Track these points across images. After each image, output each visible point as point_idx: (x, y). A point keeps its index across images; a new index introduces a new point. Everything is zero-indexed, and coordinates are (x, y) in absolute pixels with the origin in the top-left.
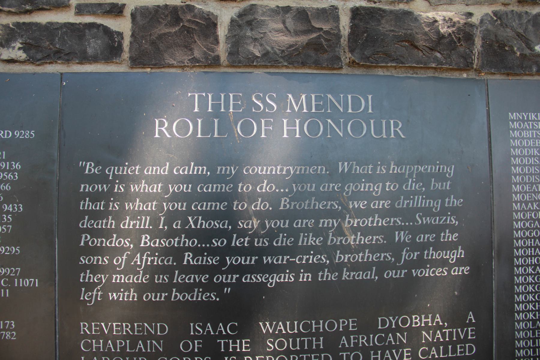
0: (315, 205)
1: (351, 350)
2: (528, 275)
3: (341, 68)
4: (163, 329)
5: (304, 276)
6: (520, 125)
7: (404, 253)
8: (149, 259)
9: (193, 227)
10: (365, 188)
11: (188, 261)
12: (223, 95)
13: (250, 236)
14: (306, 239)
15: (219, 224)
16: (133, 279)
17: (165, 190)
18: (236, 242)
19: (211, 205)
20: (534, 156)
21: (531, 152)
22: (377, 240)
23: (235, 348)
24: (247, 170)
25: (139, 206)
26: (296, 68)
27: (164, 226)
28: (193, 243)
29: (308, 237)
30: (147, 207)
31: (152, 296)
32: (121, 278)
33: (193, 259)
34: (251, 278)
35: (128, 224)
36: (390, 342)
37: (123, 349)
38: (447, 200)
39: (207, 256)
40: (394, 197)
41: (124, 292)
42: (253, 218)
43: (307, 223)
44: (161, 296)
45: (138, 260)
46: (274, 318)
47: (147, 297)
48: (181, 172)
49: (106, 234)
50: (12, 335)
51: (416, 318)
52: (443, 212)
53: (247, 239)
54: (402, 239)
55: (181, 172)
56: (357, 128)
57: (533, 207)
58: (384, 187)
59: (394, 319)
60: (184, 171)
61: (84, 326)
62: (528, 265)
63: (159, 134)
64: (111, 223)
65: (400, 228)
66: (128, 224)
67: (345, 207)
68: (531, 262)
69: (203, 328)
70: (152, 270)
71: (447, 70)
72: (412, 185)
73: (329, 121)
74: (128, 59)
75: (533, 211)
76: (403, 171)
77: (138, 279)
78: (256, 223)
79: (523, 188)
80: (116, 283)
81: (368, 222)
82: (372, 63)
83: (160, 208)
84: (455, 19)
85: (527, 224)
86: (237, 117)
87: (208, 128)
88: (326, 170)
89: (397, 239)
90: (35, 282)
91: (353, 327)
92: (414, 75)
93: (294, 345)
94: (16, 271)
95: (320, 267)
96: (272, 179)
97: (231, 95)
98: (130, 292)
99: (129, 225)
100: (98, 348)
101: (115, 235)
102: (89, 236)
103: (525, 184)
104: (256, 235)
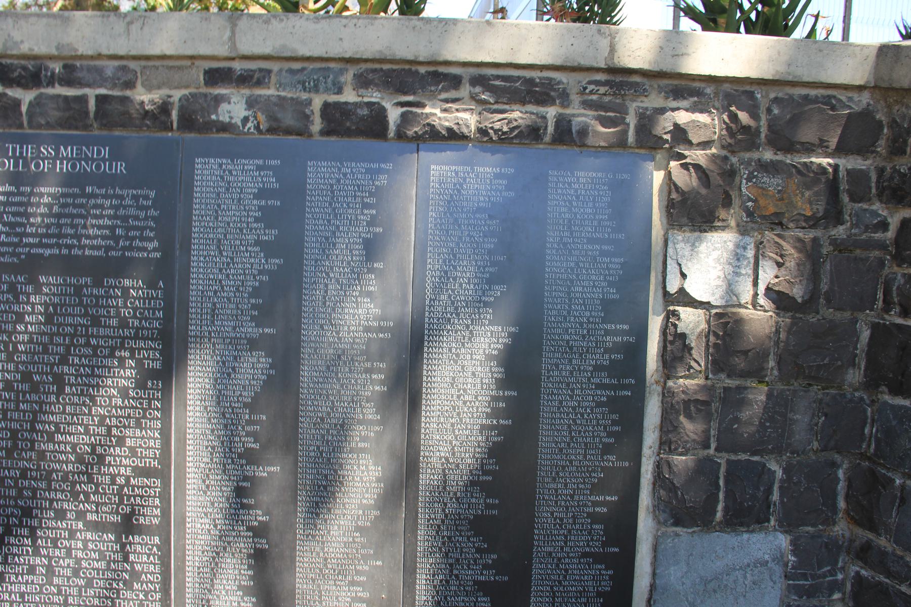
18: (29, 230)
40: (116, 208)
46: (47, 274)
52: (146, 218)
56: (98, 167)
67: (89, 213)
69: (10, 277)
72: (128, 202)
78: (39, 219)
84: (156, 100)
85: (202, 230)
86: (32, 159)
87: (16, 165)
93: (58, 290)
95: (73, 246)
96: (49, 195)
104: (39, 226)
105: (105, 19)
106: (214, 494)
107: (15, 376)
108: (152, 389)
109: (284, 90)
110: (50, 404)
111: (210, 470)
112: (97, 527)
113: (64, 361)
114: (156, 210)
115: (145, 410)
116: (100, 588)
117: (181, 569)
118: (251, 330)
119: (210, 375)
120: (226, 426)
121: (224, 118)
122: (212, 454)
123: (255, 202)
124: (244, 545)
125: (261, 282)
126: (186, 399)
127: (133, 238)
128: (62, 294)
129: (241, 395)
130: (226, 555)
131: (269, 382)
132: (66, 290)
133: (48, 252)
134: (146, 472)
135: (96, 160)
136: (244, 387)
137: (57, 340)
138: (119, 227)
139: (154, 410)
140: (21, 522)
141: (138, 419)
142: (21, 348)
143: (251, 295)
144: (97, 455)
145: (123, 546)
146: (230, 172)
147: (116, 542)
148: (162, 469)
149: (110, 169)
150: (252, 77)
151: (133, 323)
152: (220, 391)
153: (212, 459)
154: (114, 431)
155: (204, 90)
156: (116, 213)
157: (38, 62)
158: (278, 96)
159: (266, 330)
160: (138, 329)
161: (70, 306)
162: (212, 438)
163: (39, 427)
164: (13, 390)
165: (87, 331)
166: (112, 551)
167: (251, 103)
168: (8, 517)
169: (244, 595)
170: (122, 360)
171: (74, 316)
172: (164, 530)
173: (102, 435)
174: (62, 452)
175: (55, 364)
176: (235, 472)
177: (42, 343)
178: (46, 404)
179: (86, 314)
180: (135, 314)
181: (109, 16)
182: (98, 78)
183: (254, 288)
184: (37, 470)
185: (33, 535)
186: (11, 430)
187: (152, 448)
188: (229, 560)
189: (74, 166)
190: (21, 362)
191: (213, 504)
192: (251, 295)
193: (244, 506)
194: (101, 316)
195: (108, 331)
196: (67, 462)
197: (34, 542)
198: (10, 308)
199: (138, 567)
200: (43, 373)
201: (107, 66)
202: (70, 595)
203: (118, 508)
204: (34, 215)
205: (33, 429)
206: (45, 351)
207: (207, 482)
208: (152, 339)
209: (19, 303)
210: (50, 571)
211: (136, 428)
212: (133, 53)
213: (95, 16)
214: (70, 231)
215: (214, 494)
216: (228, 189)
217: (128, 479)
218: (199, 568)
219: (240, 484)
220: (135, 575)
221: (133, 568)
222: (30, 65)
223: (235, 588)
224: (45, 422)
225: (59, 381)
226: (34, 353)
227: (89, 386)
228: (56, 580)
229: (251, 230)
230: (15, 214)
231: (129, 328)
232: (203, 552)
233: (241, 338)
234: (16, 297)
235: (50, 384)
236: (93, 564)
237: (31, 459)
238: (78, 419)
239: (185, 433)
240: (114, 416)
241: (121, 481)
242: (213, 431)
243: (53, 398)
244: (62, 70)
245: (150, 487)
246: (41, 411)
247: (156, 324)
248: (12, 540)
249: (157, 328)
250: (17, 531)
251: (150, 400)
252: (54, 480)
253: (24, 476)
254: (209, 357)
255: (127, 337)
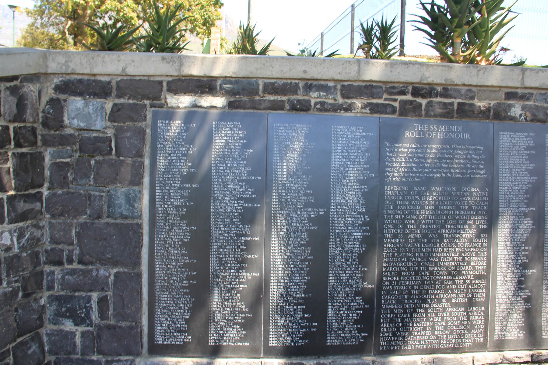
18: (426, 165)
40: (466, 155)
46: (435, 186)
52: (480, 160)
56: (457, 136)
67: (454, 157)
96: (435, 149)
105: (468, 68)
106: (508, 284)
107: (420, 236)
108: (483, 238)
109: (537, 102)
110: (436, 248)
111: (507, 273)
112: (456, 305)
113: (443, 227)
114: (484, 156)
115: (480, 248)
116: (456, 334)
117: (493, 321)
118: (525, 209)
119: (508, 230)
120: (514, 253)
121: (513, 114)
122: (508, 266)
123: (525, 152)
124: (521, 306)
125: (529, 187)
126: (497, 242)
127: (474, 169)
128: (442, 196)
129: (521, 238)
130: (513, 312)
131: (532, 232)
132: (444, 193)
133: (436, 176)
134: (479, 277)
135: (456, 132)
136: (522, 235)
137: (440, 217)
138: (468, 163)
139: (483, 247)
140: (421, 306)
141: (476, 252)
142: (423, 222)
143: (525, 193)
144: (458, 271)
145: (468, 313)
146: (514, 138)
147: (464, 311)
148: (487, 275)
149: (463, 136)
150: (525, 96)
151: (475, 208)
152: (512, 237)
153: (508, 268)
154: (466, 259)
155: (503, 101)
156: (466, 157)
157: (431, 86)
158: (535, 105)
159: (531, 209)
160: (477, 210)
161: (446, 201)
162: (509, 258)
163: (431, 259)
164: (419, 243)
165: (454, 212)
166: (463, 316)
167: (523, 108)
168: (414, 304)
169: (520, 330)
170: (470, 225)
171: (448, 206)
172: (486, 304)
173: (460, 261)
174: (442, 271)
175: (439, 229)
176: (518, 273)
177: (433, 219)
178: (435, 248)
179: (453, 205)
180: (476, 203)
181: (470, 67)
182: (458, 94)
183: (526, 190)
184: (429, 280)
185: (426, 312)
186: (417, 262)
187: (483, 265)
188: (514, 315)
189: (446, 135)
190: (423, 229)
191: (508, 289)
192: (525, 193)
193: (521, 289)
194: (460, 205)
195: (463, 212)
196: (443, 275)
197: (426, 315)
198: (418, 203)
199: (474, 322)
200: (433, 233)
201: (462, 89)
202: (442, 339)
203: (466, 295)
204: (429, 158)
205: (428, 261)
206: (435, 223)
207: (506, 279)
208: (483, 215)
209: (421, 200)
210: (433, 328)
211: (475, 256)
212: (479, 84)
213: (464, 67)
214: (445, 165)
215: (508, 284)
216: (514, 146)
217: (471, 281)
218: (501, 320)
219: (520, 279)
220: (473, 326)
221: (472, 323)
222: (427, 87)
223: (516, 327)
224: (434, 257)
225: (441, 237)
226: (429, 224)
227: (455, 238)
228: (436, 333)
229: (524, 164)
230: (419, 158)
231: (473, 210)
232: (503, 312)
233: (521, 213)
234: (421, 198)
235: (437, 238)
236: (453, 323)
237: (426, 275)
238: (449, 254)
239: (497, 257)
240: (466, 252)
241: (468, 282)
242: (509, 255)
243: (438, 245)
244: (442, 90)
245: (481, 284)
246: (432, 252)
247: (485, 208)
248: (416, 315)
249: (485, 210)
250: (418, 311)
251: (482, 243)
252: (437, 284)
253: (423, 284)
254: (507, 222)
255: (472, 215)
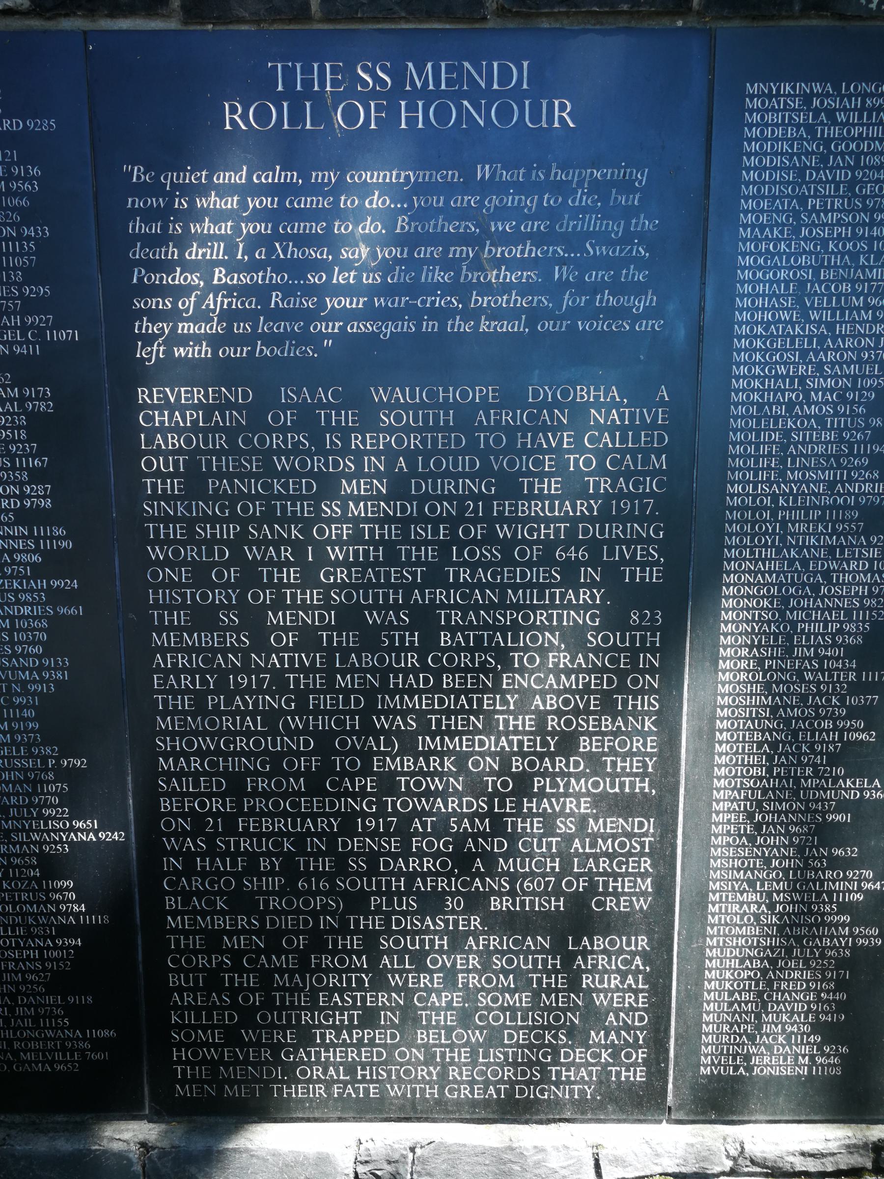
0: (443, 226)
1: (489, 429)
2: (756, 337)
3: (484, 19)
4: (245, 395)
5: (428, 325)
6: (763, 103)
7: (567, 297)
8: (226, 301)
9: (282, 256)
10: (513, 202)
11: (276, 302)
12: (316, 66)
13: (356, 269)
14: (430, 274)
15: (316, 252)
16: (204, 329)
17: (243, 205)
18: (339, 278)
19: (305, 226)
20: (782, 154)
21: (778, 147)
22: (529, 277)
23: (338, 422)
24: (352, 177)
25: (209, 228)
26: (421, 21)
27: (243, 256)
28: (282, 278)
29: (434, 270)
30: (220, 229)
31: (230, 351)
32: (189, 327)
33: (283, 300)
34: (358, 327)
35: (195, 253)
36: (545, 421)
37: (195, 422)
38: (634, 221)
39: (301, 297)
41: (194, 346)
42: (361, 244)
43: (432, 252)
44: (242, 351)
45: (211, 302)
47: (224, 352)
48: (263, 181)
49: (167, 267)
50: (48, 406)
51: (582, 390)
52: (627, 239)
53: (352, 274)
54: (564, 277)
55: (263, 181)
56: (505, 113)
57: (772, 234)
58: (541, 199)
59: (550, 389)
60: (267, 178)
61: (142, 394)
62: (757, 323)
63: (231, 125)
64: (173, 253)
65: (562, 262)
66: (195, 253)
67: (485, 231)
68: (763, 318)
70: (229, 316)
71: (650, 15)
73: (465, 103)
74: (179, 9)
75: (771, 240)
76: (570, 178)
77: (211, 329)
79: (758, 204)
80: (183, 334)
81: (517, 252)
82: (530, 8)
83: (237, 230)
85: (761, 261)
86: (337, 98)
88: (459, 177)
89: (557, 276)
90: (74, 334)
91: (494, 398)
92: (598, 27)
94: (47, 320)
97: (328, 65)
98: (201, 346)
99: (197, 255)
100: (162, 422)
101: (178, 269)
102: (143, 271)
103: (763, 197)
